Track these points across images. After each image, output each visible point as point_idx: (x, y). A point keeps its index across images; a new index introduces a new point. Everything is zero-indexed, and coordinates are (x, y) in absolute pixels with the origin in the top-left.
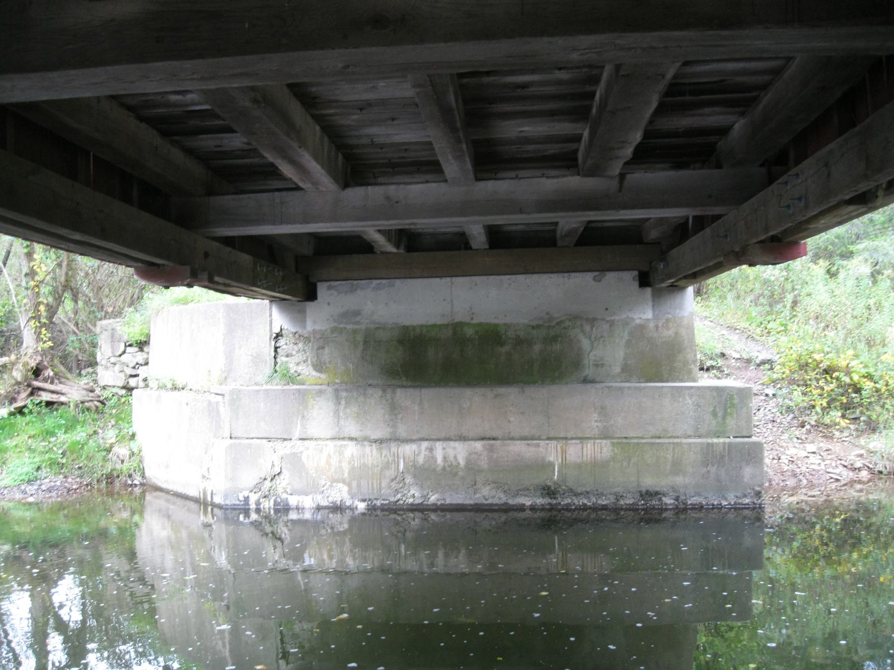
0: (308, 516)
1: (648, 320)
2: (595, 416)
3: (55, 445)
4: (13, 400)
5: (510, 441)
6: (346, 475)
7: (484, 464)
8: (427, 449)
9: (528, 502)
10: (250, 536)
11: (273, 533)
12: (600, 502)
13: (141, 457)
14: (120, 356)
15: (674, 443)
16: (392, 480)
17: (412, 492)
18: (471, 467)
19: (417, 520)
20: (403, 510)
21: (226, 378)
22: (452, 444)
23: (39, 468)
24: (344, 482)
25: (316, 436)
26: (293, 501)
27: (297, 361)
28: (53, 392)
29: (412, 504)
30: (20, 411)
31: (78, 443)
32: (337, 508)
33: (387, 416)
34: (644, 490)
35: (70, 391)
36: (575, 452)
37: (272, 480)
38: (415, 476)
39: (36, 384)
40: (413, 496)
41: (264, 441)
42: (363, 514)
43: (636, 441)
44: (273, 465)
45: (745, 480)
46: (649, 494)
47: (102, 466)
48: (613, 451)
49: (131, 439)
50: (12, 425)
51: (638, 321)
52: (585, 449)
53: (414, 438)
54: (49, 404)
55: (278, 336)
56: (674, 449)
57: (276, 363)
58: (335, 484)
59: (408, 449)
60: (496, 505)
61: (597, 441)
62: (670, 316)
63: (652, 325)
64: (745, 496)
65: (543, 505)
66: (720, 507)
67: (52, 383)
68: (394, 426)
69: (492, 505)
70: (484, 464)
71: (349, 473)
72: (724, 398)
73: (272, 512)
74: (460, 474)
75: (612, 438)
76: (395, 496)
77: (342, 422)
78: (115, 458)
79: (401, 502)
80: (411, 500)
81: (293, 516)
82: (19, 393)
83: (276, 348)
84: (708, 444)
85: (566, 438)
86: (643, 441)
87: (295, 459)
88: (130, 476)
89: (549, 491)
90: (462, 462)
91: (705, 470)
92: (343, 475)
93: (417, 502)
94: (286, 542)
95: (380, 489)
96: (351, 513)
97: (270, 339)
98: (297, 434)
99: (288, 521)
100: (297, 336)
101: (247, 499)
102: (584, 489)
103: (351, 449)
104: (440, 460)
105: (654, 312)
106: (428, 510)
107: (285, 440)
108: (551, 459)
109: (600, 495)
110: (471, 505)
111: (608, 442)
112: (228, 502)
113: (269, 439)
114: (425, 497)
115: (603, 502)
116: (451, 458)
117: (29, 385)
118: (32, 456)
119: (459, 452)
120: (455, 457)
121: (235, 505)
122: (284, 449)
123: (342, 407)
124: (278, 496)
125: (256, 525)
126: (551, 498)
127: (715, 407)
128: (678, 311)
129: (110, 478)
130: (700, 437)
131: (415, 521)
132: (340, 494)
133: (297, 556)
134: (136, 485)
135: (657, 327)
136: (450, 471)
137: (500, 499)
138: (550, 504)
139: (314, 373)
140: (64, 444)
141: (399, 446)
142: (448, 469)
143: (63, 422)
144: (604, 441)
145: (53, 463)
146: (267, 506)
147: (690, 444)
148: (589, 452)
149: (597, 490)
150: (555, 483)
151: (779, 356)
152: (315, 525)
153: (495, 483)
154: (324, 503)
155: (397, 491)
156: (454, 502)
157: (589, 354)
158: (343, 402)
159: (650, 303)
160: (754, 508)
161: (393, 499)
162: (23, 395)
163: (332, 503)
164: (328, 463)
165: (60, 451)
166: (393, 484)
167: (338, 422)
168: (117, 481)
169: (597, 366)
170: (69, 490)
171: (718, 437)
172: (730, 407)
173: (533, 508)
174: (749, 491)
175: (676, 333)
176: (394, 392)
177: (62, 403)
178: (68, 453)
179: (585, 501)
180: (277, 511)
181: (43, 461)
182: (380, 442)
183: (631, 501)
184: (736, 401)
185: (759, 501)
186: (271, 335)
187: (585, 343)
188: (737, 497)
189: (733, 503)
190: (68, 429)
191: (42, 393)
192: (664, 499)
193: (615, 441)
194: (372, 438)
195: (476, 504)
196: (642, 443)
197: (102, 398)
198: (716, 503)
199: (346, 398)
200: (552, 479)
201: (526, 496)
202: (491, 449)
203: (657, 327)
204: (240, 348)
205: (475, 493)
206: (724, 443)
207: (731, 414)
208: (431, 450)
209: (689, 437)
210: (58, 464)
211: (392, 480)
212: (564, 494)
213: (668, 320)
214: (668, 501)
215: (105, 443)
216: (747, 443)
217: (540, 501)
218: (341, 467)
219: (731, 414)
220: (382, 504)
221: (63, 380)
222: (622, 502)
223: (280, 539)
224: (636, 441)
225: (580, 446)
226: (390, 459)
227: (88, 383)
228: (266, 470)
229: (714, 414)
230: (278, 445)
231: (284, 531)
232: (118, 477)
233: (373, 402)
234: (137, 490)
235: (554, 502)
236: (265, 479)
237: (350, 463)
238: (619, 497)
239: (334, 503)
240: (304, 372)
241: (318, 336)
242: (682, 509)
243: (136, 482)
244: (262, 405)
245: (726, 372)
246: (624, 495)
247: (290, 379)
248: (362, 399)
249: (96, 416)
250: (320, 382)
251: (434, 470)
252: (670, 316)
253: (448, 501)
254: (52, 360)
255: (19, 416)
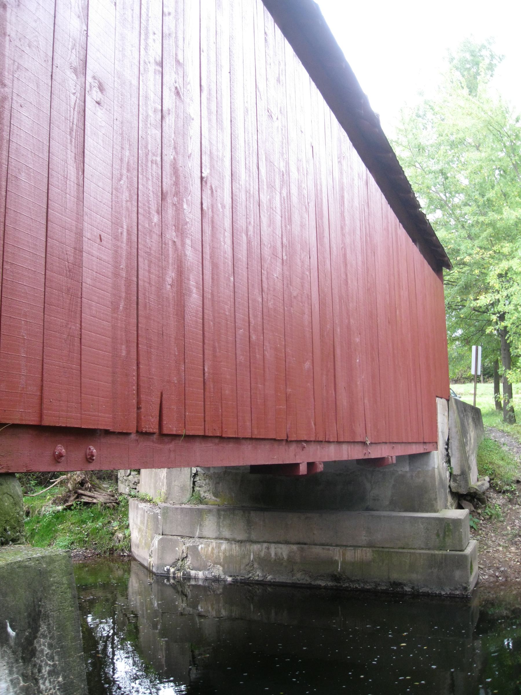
0: (200, 583)
1: (406, 472)
2: (364, 533)
3: (84, 530)
4: (66, 501)
5: (313, 546)
6: (222, 560)
7: (298, 558)
8: (266, 547)
9: (323, 583)
10: (170, 592)
11: (182, 592)
12: (365, 587)
13: (130, 539)
14: (128, 476)
15: (410, 553)
16: (247, 565)
17: (258, 573)
18: (291, 560)
19: (260, 590)
20: (252, 583)
21: (167, 498)
22: (280, 545)
23: (73, 543)
24: (220, 565)
25: (207, 536)
26: (193, 573)
27: (205, 490)
28: (90, 497)
29: (257, 580)
30: (69, 508)
31: (97, 529)
32: (216, 580)
33: (246, 527)
34: (392, 581)
35: (99, 496)
36: (350, 555)
37: (182, 560)
38: (259, 564)
39: (80, 491)
40: (258, 576)
41: (179, 538)
42: (230, 584)
43: (387, 550)
44: (183, 552)
45: (456, 579)
46: (396, 584)
47: (108, 543)
48: (373, 555)
49: (126, 528)
50: (64, 516)
51: (400, 473)
52: (356, 553)
53: (260, 540)
54: (86, 504)
55: (196, 475)
56: (410, 556)
57: (193, 491)
58: (215, 565)
59: (256, 547)
60: (305, 584)
61: (364, 549)
62: (420, 469)
63: (409, 475)
64: (456, 589)
65: (331, 586)
66: (440, 595)
67: (90, 491)
68: (250, 533)
69: (302, 584)
70: (298, 558)
71: (223, 559)
72: (443, 525)
73: (182, 579)
74: (284, 564)
75: (375, 547)
76: (248, 575)
77: (221, 529)
78: (116, 539)
79: (252, 579)
80: (257, 578)
81: (193, 583)
82: (69, 497)
83: (194, 483)
84: (432, 554)
85: (347, 546)
86: (392, 550)
87: (194, 549)
88: (123, 550)
89: (336, 578)
90: (285, 557)
91: (430, 571)
92: (220, 560)
93: (260, 579)
94: (189, 597)
95: (240, 570)
96: (224, 583)
97: (191, 477)
98: (197, 534)
99: (190, 585)
100: (205, 475)
101: (168, 570)
102: (356, 578)
103: (224, 546)
104: (273, 555)
105: (410, 467)
106: (266, 584)
107: (191, 537)
108: (337, 558)
109: (365, 582)
110: (290, 583)
111: (371, 549)
112: (159, 572)
113: (182, 537)
114: (265, 577)
115: (368, 587)
116: (279, 554)
117: (76, 493)
118: (70, 535)
119: (284, 551)
120: (282, 554)
121: (162, 573)
122: (189, 543)
123: (221, 520)
124: (185, 570)
125: (173, 586)
126: (337, 582)
127: (438, 531)
128: (425, 467)
129: (112, 551)
130: (429, 549)
131: (259, 591)
132: (218, 571)
133: (194, 606)
134: (125, 556)
135: (412, 476)
136: (278, 562)
137: (307, 580)
138: (336, 586)
139: (213, 498)
140: (89, 529)
141: (250, 545)
142: (277, 560)
143: (93, 515)
144: (368, 549)
145: (82, 541)
146: (179, 575)
147: (420, 554)
148: (359, 555)
149: (364, 579)
150: (339, 573)
151: (66, 591)
152: (205, 589)
153: (304, 571)
154: (209, 576)
155: (249, 572)
156: (281, 581)
157: (370, 492)
158: (222, 517)
159: (408, 461)
160: (463, 598)
161: (247, 577)
162: (72, 498)
163: (214, 576)
164: (212, 552)
165: (86, 534)
166: (247, 568)
167: (219, 529)
168: (115, 552)
169: (374, 500)
170: (86, 557)
171: (441, 550)
172: (448, 531)
173: (325, 588)
174: (459, 586)
175: (424, 481)
176: (249, 513)
177: (94, 503)
178: (90, 535)
179: (357, 586)
180: (184, 579)
181: (75, 539)
182: (241, 542)
183: (384, 588)
184: (451, 527)
185: (466, 593)
186: (191, 474)
187: (368, 486)
188: (451, 590)
189: (448, 593)
190: (95, 519)
191: (84, 497)
192: (405, 587)
193: (374, 549)
194: (237, 539)
195: (293, 583)
196: (391, 552)
197: (117, 501)
198: (437, 593)
199: (224, 515)
200: (337, 570)
201: (322, 580)
202: (302, 550)
203: (412, 476)
204: (175, 481)
205: (293, 577)
206: (442, 555)
207: (448, 536)
208: (268, 548)
209: (422, 549)
210: (84, 541)
211: (247, 565)
212: (345, 580)
213: (419, 472)
214: (407, 589)
215: (113, 529)
216: (458, 555)
217: (330, 584)
218: (219, 556)
219: (448, 536)
220: (241, 579)
221: (97, 489)
222: (379, 588)
223: (186, 596)
224: (387, 550)
225: (353, 551)
226: (246, 552)
227: (112, 491)
228: (179, 555)
229: (438, 535)
230: (186, 540)
231: (188, 591)
232: (116, 550)
233: (238, 518)
234: (126, 559)
235: (339, 585)
236: (179, 560)
237: (224, 553)
238: (378, 585)
239: (215, 576)
240: (207, 497)
241: (216, 476)
242: (416, 595)
243: (125, 554)
244: (179, 517)
245: (517, 495)
246: (380, 583)
247: (201, 501)
248: (232, 516)
249: (113, 512)
250: (216, 503)
251: (270, 561)
252: (420, 469)
253: (277, 580)
254: (91, 477)
255: (68, 511)
